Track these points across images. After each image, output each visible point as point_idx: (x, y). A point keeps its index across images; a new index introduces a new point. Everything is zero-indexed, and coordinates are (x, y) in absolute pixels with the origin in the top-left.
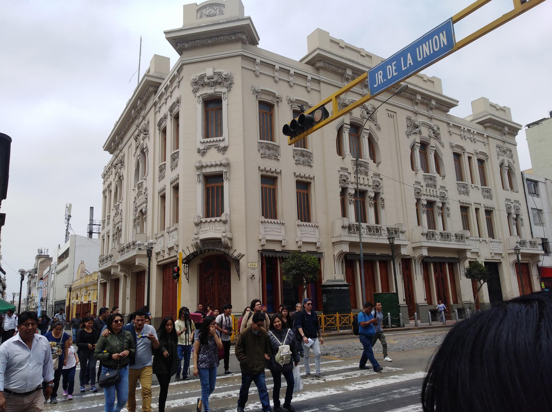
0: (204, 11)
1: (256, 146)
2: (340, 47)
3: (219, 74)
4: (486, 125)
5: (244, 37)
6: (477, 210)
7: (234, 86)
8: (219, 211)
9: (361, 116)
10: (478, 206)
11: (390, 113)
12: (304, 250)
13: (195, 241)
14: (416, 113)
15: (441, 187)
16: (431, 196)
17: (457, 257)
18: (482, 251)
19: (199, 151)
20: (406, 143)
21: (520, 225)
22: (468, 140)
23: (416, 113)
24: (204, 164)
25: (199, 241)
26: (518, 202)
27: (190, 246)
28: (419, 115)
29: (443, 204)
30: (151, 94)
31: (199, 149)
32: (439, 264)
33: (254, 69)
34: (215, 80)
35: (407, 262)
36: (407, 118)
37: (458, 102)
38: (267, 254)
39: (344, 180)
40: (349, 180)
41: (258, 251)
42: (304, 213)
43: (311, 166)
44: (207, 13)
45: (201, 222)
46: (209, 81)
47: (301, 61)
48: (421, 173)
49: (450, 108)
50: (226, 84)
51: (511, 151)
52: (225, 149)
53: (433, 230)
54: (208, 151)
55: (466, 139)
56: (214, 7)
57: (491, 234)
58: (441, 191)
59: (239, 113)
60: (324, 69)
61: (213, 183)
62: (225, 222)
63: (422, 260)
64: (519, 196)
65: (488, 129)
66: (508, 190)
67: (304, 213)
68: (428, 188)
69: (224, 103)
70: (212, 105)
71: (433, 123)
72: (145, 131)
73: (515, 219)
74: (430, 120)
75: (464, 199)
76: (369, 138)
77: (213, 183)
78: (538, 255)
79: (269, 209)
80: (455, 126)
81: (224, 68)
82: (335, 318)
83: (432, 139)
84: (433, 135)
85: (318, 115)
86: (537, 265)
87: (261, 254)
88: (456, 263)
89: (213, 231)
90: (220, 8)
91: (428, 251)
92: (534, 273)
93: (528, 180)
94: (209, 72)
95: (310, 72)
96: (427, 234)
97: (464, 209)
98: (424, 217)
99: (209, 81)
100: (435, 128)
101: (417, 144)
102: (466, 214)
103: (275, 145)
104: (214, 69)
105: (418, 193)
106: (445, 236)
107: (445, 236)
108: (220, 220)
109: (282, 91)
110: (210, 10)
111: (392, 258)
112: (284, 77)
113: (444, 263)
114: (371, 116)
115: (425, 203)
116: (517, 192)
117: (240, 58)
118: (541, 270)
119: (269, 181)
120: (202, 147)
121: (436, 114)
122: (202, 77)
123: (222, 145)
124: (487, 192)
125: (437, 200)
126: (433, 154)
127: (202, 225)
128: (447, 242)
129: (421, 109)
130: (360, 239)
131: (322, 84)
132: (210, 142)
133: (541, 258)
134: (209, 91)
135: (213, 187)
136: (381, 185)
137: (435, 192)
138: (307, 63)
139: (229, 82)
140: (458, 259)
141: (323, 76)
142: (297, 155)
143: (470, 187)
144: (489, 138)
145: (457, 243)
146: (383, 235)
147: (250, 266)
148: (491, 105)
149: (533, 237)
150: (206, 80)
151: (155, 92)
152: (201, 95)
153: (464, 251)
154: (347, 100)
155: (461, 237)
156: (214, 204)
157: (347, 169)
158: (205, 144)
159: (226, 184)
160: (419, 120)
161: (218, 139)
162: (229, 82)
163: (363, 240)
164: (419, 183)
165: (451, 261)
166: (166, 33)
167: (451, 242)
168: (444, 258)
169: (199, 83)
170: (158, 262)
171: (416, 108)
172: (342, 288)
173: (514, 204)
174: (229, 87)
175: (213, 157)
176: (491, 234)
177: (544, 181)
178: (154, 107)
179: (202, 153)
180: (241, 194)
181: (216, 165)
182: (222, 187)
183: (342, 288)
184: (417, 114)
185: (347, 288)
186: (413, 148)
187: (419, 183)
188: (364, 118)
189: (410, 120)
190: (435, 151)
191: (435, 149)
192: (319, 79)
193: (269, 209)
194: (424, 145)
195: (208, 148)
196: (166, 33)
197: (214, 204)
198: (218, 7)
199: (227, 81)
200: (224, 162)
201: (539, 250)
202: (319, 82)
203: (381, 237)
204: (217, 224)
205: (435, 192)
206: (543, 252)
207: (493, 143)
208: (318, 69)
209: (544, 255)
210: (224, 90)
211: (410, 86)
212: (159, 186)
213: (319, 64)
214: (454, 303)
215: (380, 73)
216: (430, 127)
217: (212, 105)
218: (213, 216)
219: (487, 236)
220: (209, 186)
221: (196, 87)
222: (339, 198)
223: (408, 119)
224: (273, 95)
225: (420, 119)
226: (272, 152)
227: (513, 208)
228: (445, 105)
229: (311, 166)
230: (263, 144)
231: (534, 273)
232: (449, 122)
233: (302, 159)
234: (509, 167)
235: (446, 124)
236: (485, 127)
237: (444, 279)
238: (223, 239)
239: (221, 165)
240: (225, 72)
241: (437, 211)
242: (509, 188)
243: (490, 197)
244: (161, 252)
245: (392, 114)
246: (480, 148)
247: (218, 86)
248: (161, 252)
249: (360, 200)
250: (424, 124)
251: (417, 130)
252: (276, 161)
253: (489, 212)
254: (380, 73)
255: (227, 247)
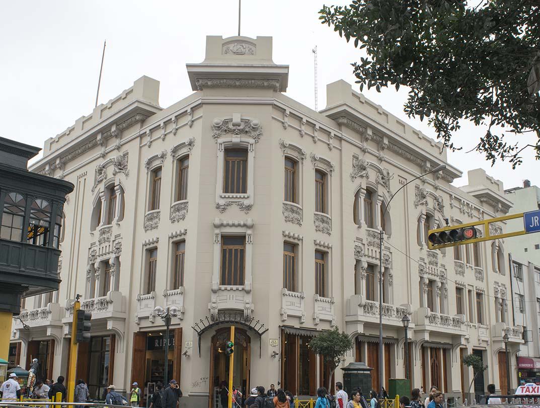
0: (231, 47)
1: (281, 208)
2: (360, 101)
3: (247, 122)
4: (482, 200)
5: (278, 85)
6: (470, 291)
7: (262, 137)
8: (239, 279)
9: (376, 181)
10: (471, 288)
11: (401, 179)
12: (319, 328)
13: (256, 319)
14: (364, 151)
15: (442, 265)
16: (373, 258)
17: (395, 337)
18: (474, 337)
19: (218, 207)
20: (415, 213)
21: (387, 283)
22: (466, 214)
23: (364, 151)
24: (225, 223)
25: (216, 311)
26: (504, 285)
27: (204, 319)
28: (367, 154)
29: (386, 269)
30: (137, 122)
31: (218, 204)
32: (435, 350)
33: (313, 135)
34: (241, 127)
35: (408, 346)
36: (353, 156)
37: (287, 67)
38: (288, 331)
39: (358, 252)
40: (363, 252)
41: (280, 326)
42: (321, 289)
43: (329, 234)
44: (235, 50)
45: (220, 289)
46: (234, 128)
47: (321, 112)
48: (364, 226)
49: (453, 178)
50: (253, 134)
51: (501, 229)
52: (249, 208)
53: (372, 302)
54: (229, 208)
55: (464, 213)
56: (243, 44)
57: (480, 320)
58: (441, 269)
59: (265, 170)
60: (347, 126)
61: (233, 247)
62: (248, 292)
63: (422, 345)
64: (505, 279)
65: (484, 204)
66: (497, 272)
67: (321, 289)
68: (371, 248)
69: (251, 156)
70: (236, 155)
71: (383, 166)
72: (120, 164)
73: (501, 305)
74: (423, 183)
75: (460, 279)
76: (381, 206)
77: (233, 247)
78: (519, 344)
79: (291, 282)
80: (296, 116)
81: (256, 116)
82: (309, 404)
83: (379, 186)
84: (437, 207)
85: (469, 234)
86: (516, 355)
87: (282, 330)
88: (450, 349)
89: (232, 300)
90: (251, 47)
91: (430, 335)
92: (513, 362)
93: (514, 262)
94: (237, 119)
95: (329, 125)
96: (365, 306)
97: (459, 290)
98: (363, 283)
99: (234, 128)
100: (385, 173)
101: (362, 190)
102: (292, 255)
103: (298, 208)
104: (241, 116)
105: (422, 270)
106: (445, 320)
107: (445, 320)
108: (243, 289)
109: (306, 146)
110: (239, 46)
111: (452, 346)
112: (295, 124)
113: (439, 349)
114: (385, 180)
115: (366, 266)
116: (505, 275)
117: (271, 107)
118: (519, 360)
119: (291, 246)
120: (222, 202)
121: (440, 184)
122: (226, 122)
123: (246, 202)
124: (480, 273)
125: (437, 279)
126: (379, 205)
127: (221, 293)
128: (446, 327)
129: (370, 146)
130: (381, 321)
131: (426, 184)
132: (233, 197)
133: (522, 347)
134: (236, 139)
135: (230, 250)
136: (390, 260)
137: (436, 270)
138: (329, 116)
139: (258, 133)
140: (452, 345)
141: (346, 134)
142: (317, 220)
143: (465, 267)
144: (343, 141)
145: (454, 328)
146: (393, 316)
147: (272, 342)
148: (353, 94)
149: (514, 325)
150: (231, 126)
151: (143, 122)
152: (224, 143)
153: (459, 337)
154: (366, 163)
155: (388, 310)
156: (233, 270)
157: (362, 240)
158: (225, 200)
159: (249, 249)
160: (427, 190)
161: (242, 195)
162: (258, 133)
163: (382, 323)
164: (424, 260)
165: (446, 347)
166: (188, 66)
167: (449, 327)
168: (440, 343)
169: (223, 128)
170: (140, 328)
171: (366, 145)
172: (365, 372)
173: (501, 288)
174: (257, 138)
175: (234, 218)
176: (480, 320)
177: (527, 264)
178: (139, 138)
179: (222, 209)
180: (263, 262)
181: (239, 225)
182: (243, 252)
183: (365, 372)
184: (365, 152)
185: (369, 372)
186: (357, 195)
187: (423, 259)
188: (379, 183)
189: (418, 188)
190: (383, 201)
191: (382, 199)
192: (340, 136)
193: (291, 282)
194: (370, 193)
195: (229, 205)
196: (188, 66)
197: (233, 270)
198: (247, 45)
199: (255, 131)
200: (249, 223)
201: (519, 339)
202: (340, 139)
203: (391, 318)
204: (238, 293)
205: (436, 270)
206: (523, 341)
207: (349, 151)
208: (340, 125)
209: (523, 344)
210: (252, 141)
211: (447, 167)
212: (145, 237)
213: (341, 120)
214: (445, 392)
215: (536, 218)
216: (380, 171)
217: (236, 155)
218: (229, 284)
219: (477, 322)
220: (225, 247)
221: (217, 132)
222: (354, 267)
223: (355, 157)
224: (299, 151)
225: (368, 159)
226: (295, 215)
227: (499, 292)
228: (450, 174)
229: (329, 234)
230: (430, 253)
231: (513, 362)
232: (451, 193)
233: (322, 225)
234: (499, 247)
235: (448, 196)
236: (481, 202)
237: (438, 367)
238: (245, 312)
239: (245, 225)
240: (254, 121)
241: (436, 291)
242: (497, 270)
243: (481, 279)
244: (151, 317)
245: (404, 180)
246: (321, 151)
247: (243, 135)
248: (151, 317)
249: (374, 276)
250: (372, 166)
251: (364, 172)
252: (298, 226)
253: (479, 295)
254: (536, 218)
255: (248, 319)
